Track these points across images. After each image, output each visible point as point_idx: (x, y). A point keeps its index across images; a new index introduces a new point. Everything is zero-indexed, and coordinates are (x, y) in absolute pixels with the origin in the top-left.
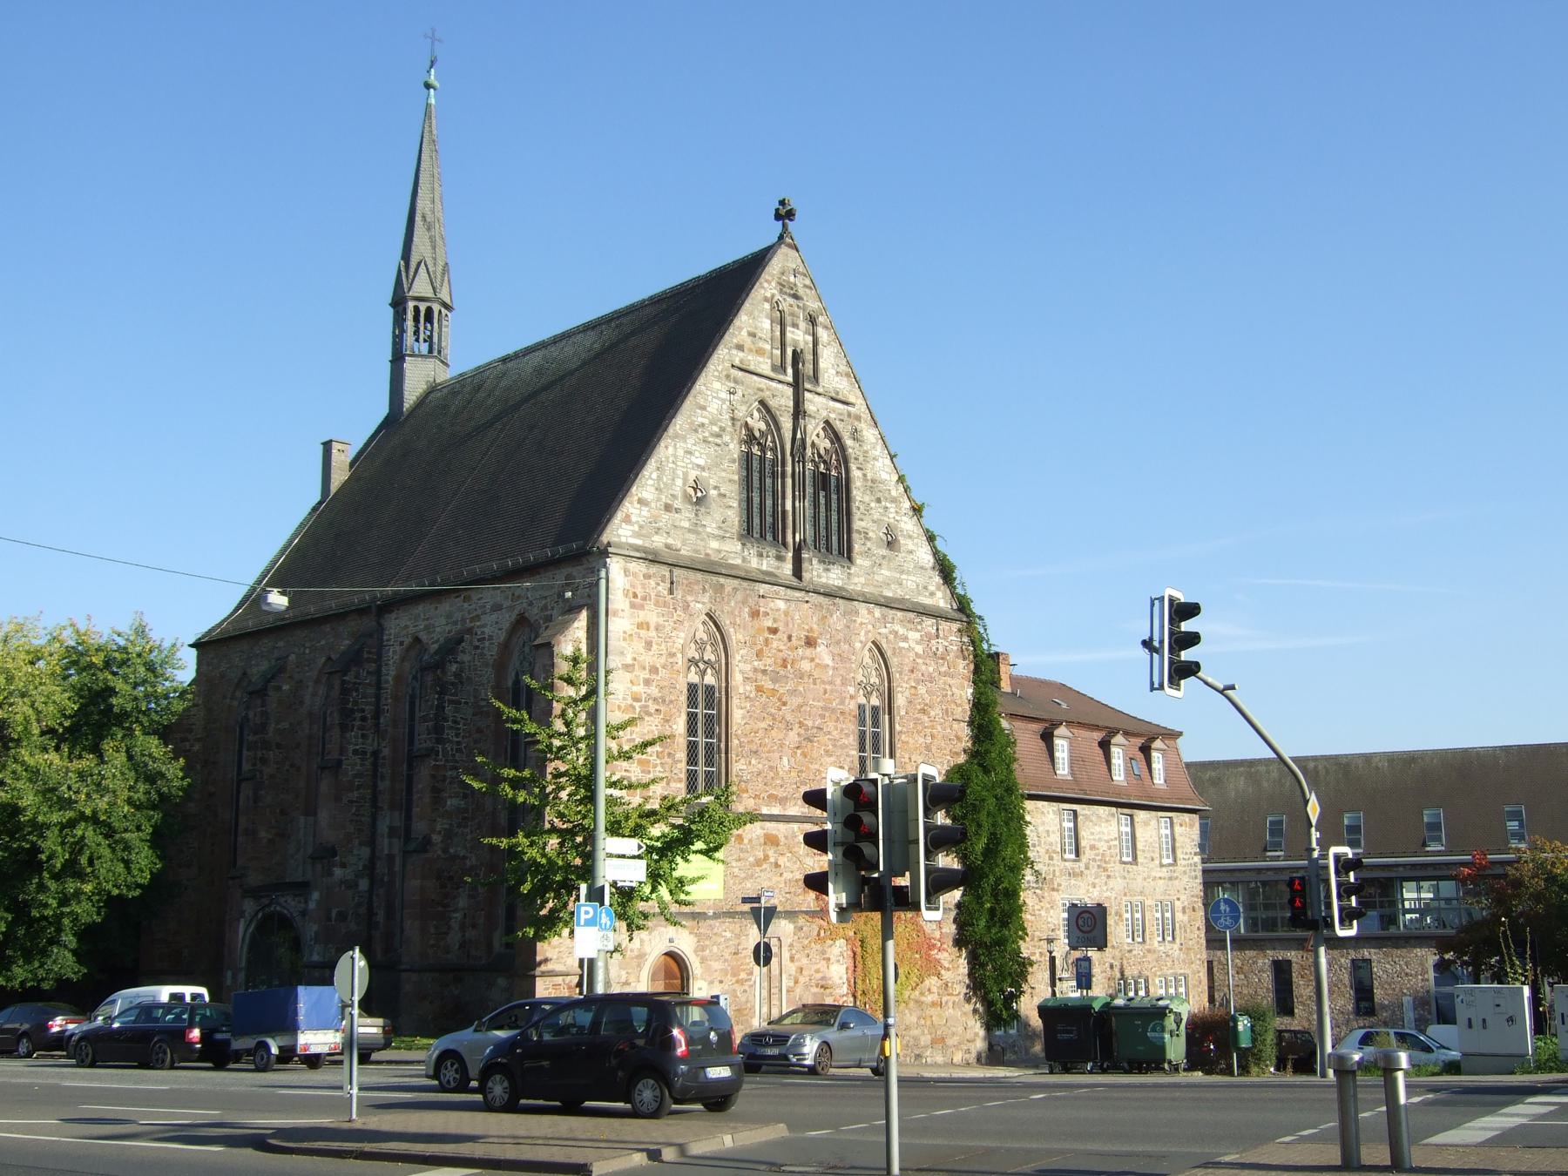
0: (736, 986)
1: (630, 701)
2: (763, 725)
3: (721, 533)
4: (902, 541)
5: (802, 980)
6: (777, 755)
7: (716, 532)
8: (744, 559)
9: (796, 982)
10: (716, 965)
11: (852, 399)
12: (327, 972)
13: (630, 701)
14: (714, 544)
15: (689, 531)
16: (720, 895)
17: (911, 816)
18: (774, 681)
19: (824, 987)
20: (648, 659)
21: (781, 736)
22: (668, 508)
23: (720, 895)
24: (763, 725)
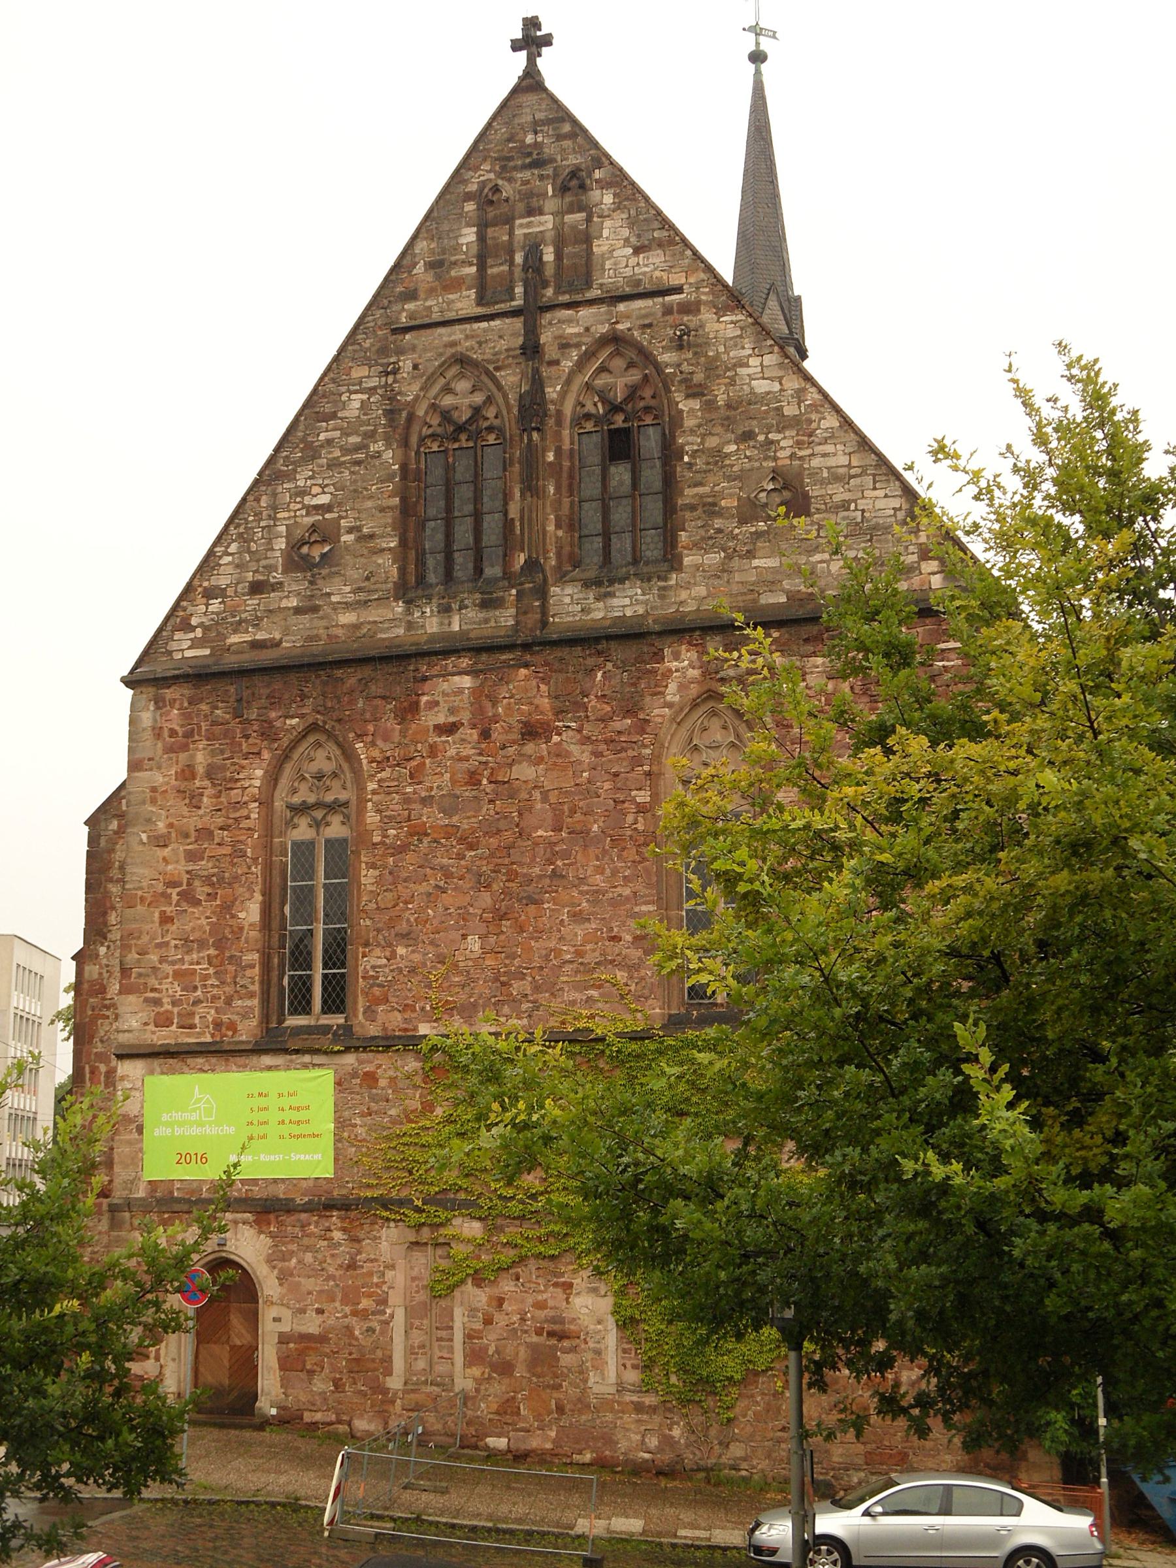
0: (353, 1321)
1: (160, 887)
2: (424, 888)
3: (362, 596)
4: (814, 491)
5: (500, 1320)
6: (456, 935)
7: (351, 598)
8: (410, 625)
9: (488, 1321)
10: (309, 1284)
11: (677, 279)
12: (280, 465)
13: (160, 887)
14: (348, 618)
15: (298, 611)
16: (326, 1170)
17: (309, 953)
18: (448, 813)
19: (562, 1336)
20: (193, 822)
21: (464, 900)
22: (257, 588)
23: (326, 1170)
24: (424, 888)
